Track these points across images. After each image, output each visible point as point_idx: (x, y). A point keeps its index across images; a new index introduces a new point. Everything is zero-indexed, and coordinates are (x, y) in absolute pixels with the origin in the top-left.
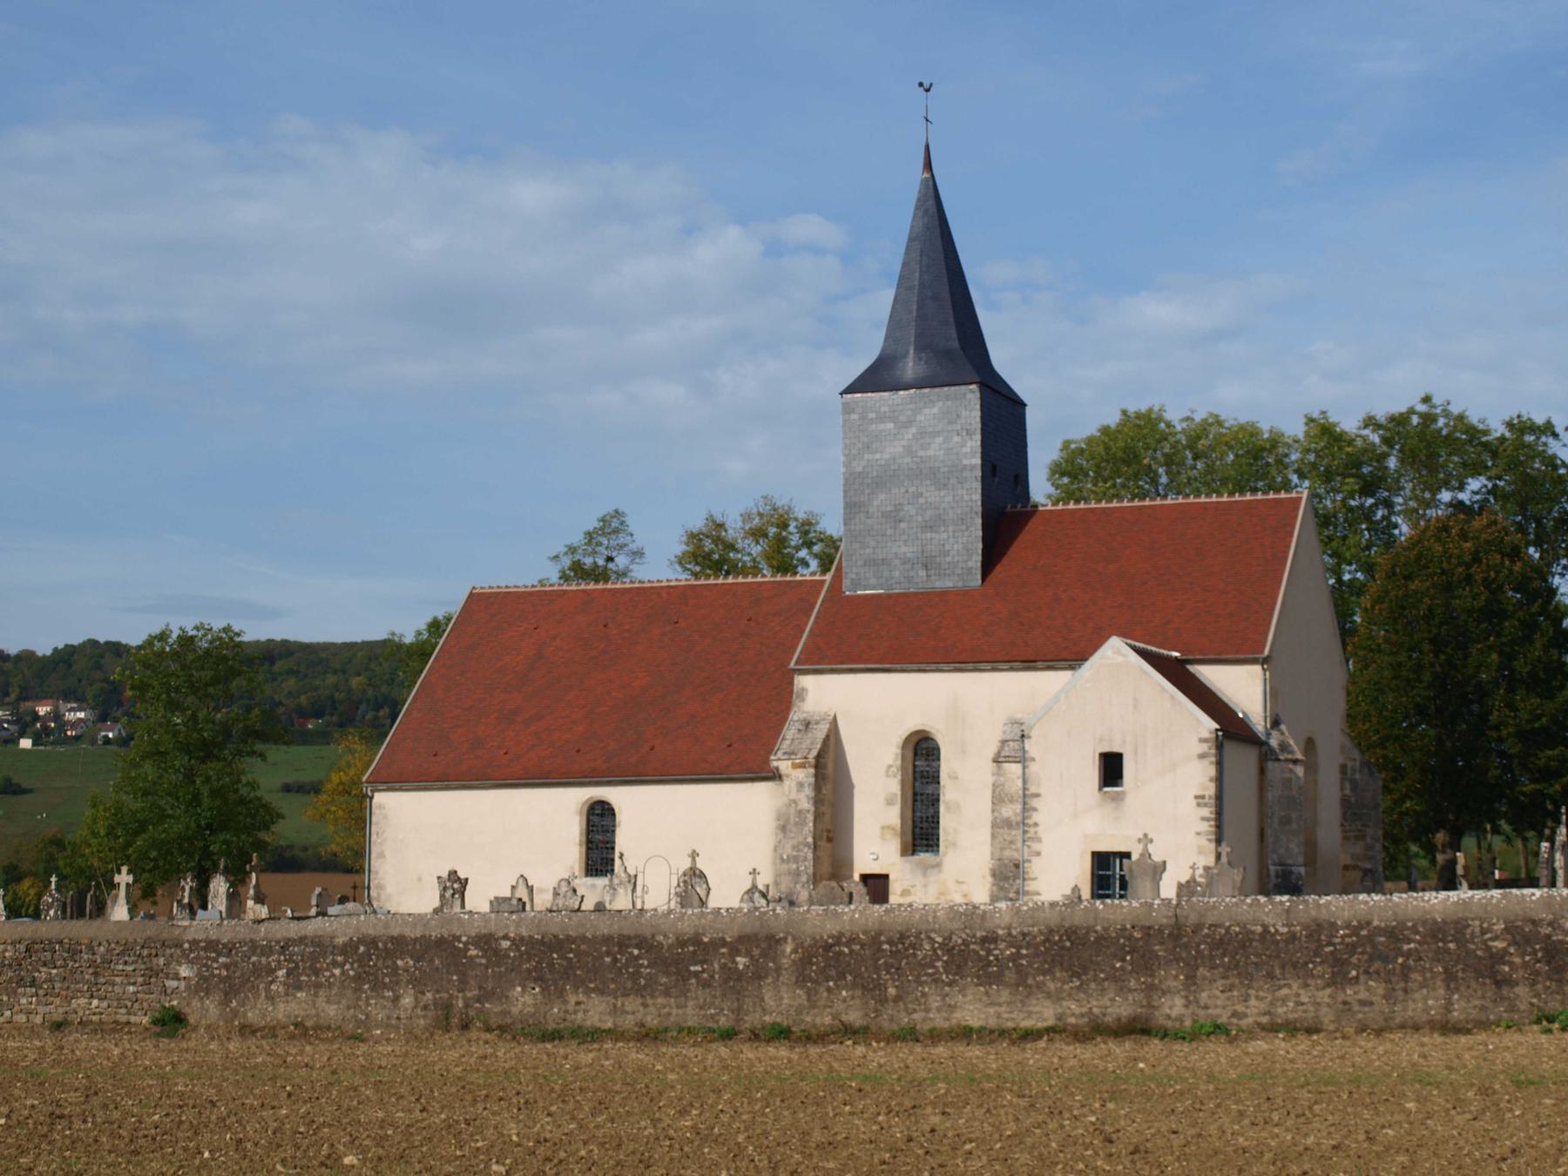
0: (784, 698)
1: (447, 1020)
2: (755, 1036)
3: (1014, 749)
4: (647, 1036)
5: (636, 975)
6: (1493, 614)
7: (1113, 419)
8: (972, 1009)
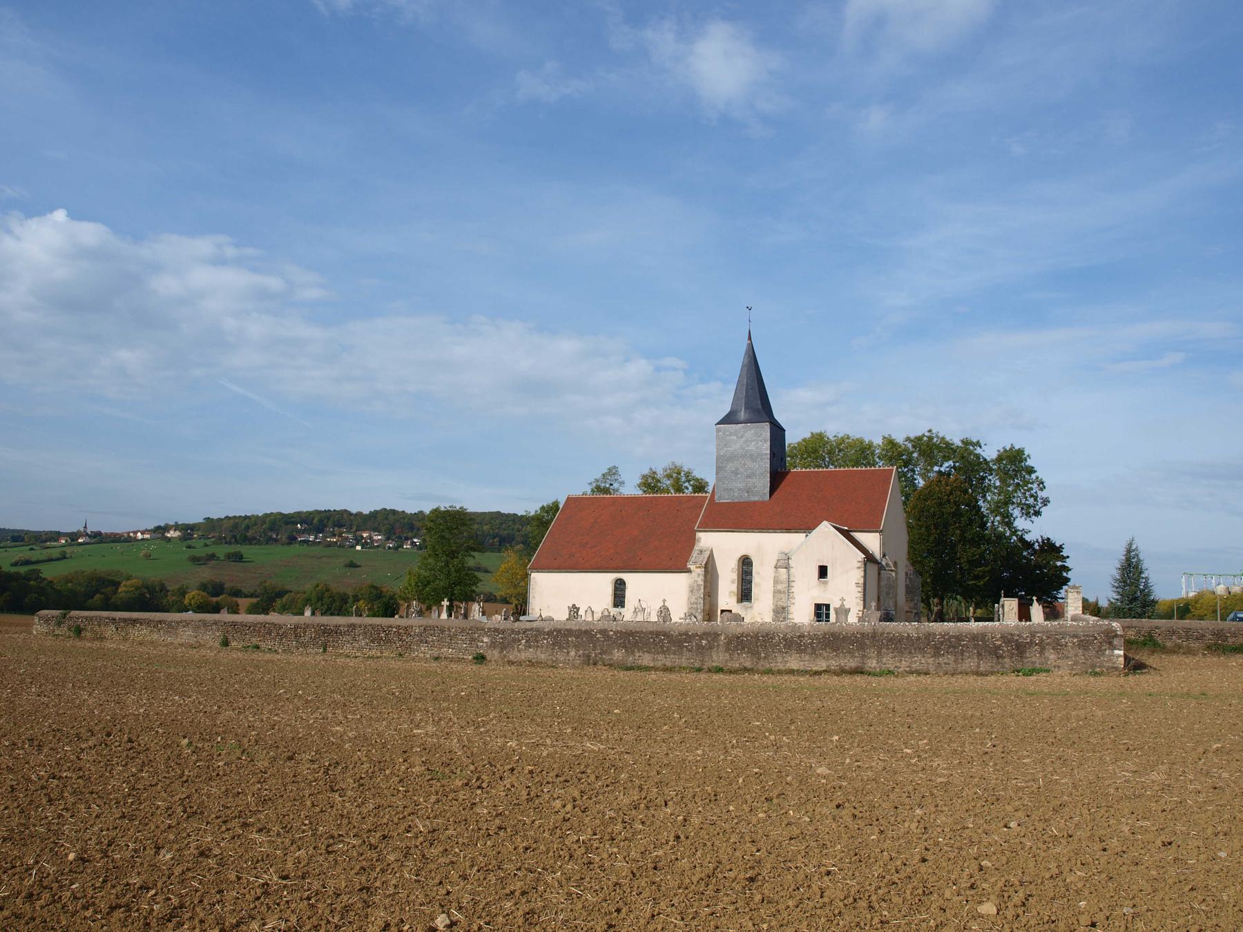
0: (692, 541)
1: (589, 661)
2: (710, 671)
3: (784, 562)
4: (666, 669)
5: (662, 647)
6: (958, 514)
7: (808, 435)
8: (794, 663)
